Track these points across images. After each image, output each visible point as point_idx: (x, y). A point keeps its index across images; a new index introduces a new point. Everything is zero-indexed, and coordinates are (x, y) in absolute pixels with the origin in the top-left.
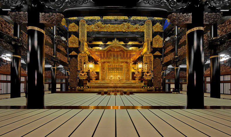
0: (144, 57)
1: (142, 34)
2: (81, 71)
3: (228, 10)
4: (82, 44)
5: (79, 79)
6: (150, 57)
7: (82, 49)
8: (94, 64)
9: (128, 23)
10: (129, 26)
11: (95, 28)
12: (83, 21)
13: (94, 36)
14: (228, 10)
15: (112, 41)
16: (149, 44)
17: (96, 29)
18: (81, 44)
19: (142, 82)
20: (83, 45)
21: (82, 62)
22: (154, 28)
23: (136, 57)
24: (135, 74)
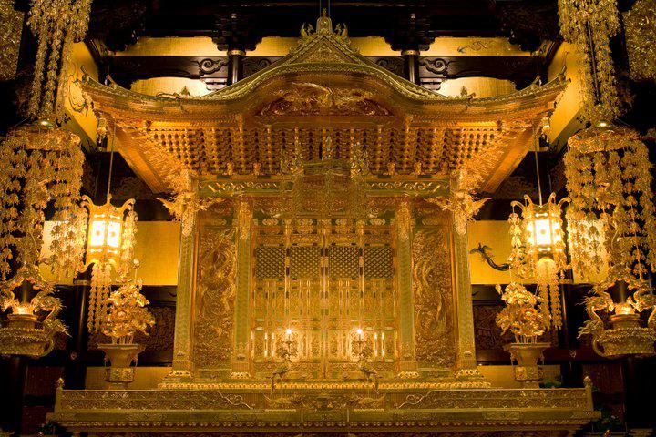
4: (49, 51)
7: (43, 92)
15: (298, 35)
16: (603, 53)
18: (41, 54)
20: (53, 64)
21: (32, 200)
24: (503, 304)
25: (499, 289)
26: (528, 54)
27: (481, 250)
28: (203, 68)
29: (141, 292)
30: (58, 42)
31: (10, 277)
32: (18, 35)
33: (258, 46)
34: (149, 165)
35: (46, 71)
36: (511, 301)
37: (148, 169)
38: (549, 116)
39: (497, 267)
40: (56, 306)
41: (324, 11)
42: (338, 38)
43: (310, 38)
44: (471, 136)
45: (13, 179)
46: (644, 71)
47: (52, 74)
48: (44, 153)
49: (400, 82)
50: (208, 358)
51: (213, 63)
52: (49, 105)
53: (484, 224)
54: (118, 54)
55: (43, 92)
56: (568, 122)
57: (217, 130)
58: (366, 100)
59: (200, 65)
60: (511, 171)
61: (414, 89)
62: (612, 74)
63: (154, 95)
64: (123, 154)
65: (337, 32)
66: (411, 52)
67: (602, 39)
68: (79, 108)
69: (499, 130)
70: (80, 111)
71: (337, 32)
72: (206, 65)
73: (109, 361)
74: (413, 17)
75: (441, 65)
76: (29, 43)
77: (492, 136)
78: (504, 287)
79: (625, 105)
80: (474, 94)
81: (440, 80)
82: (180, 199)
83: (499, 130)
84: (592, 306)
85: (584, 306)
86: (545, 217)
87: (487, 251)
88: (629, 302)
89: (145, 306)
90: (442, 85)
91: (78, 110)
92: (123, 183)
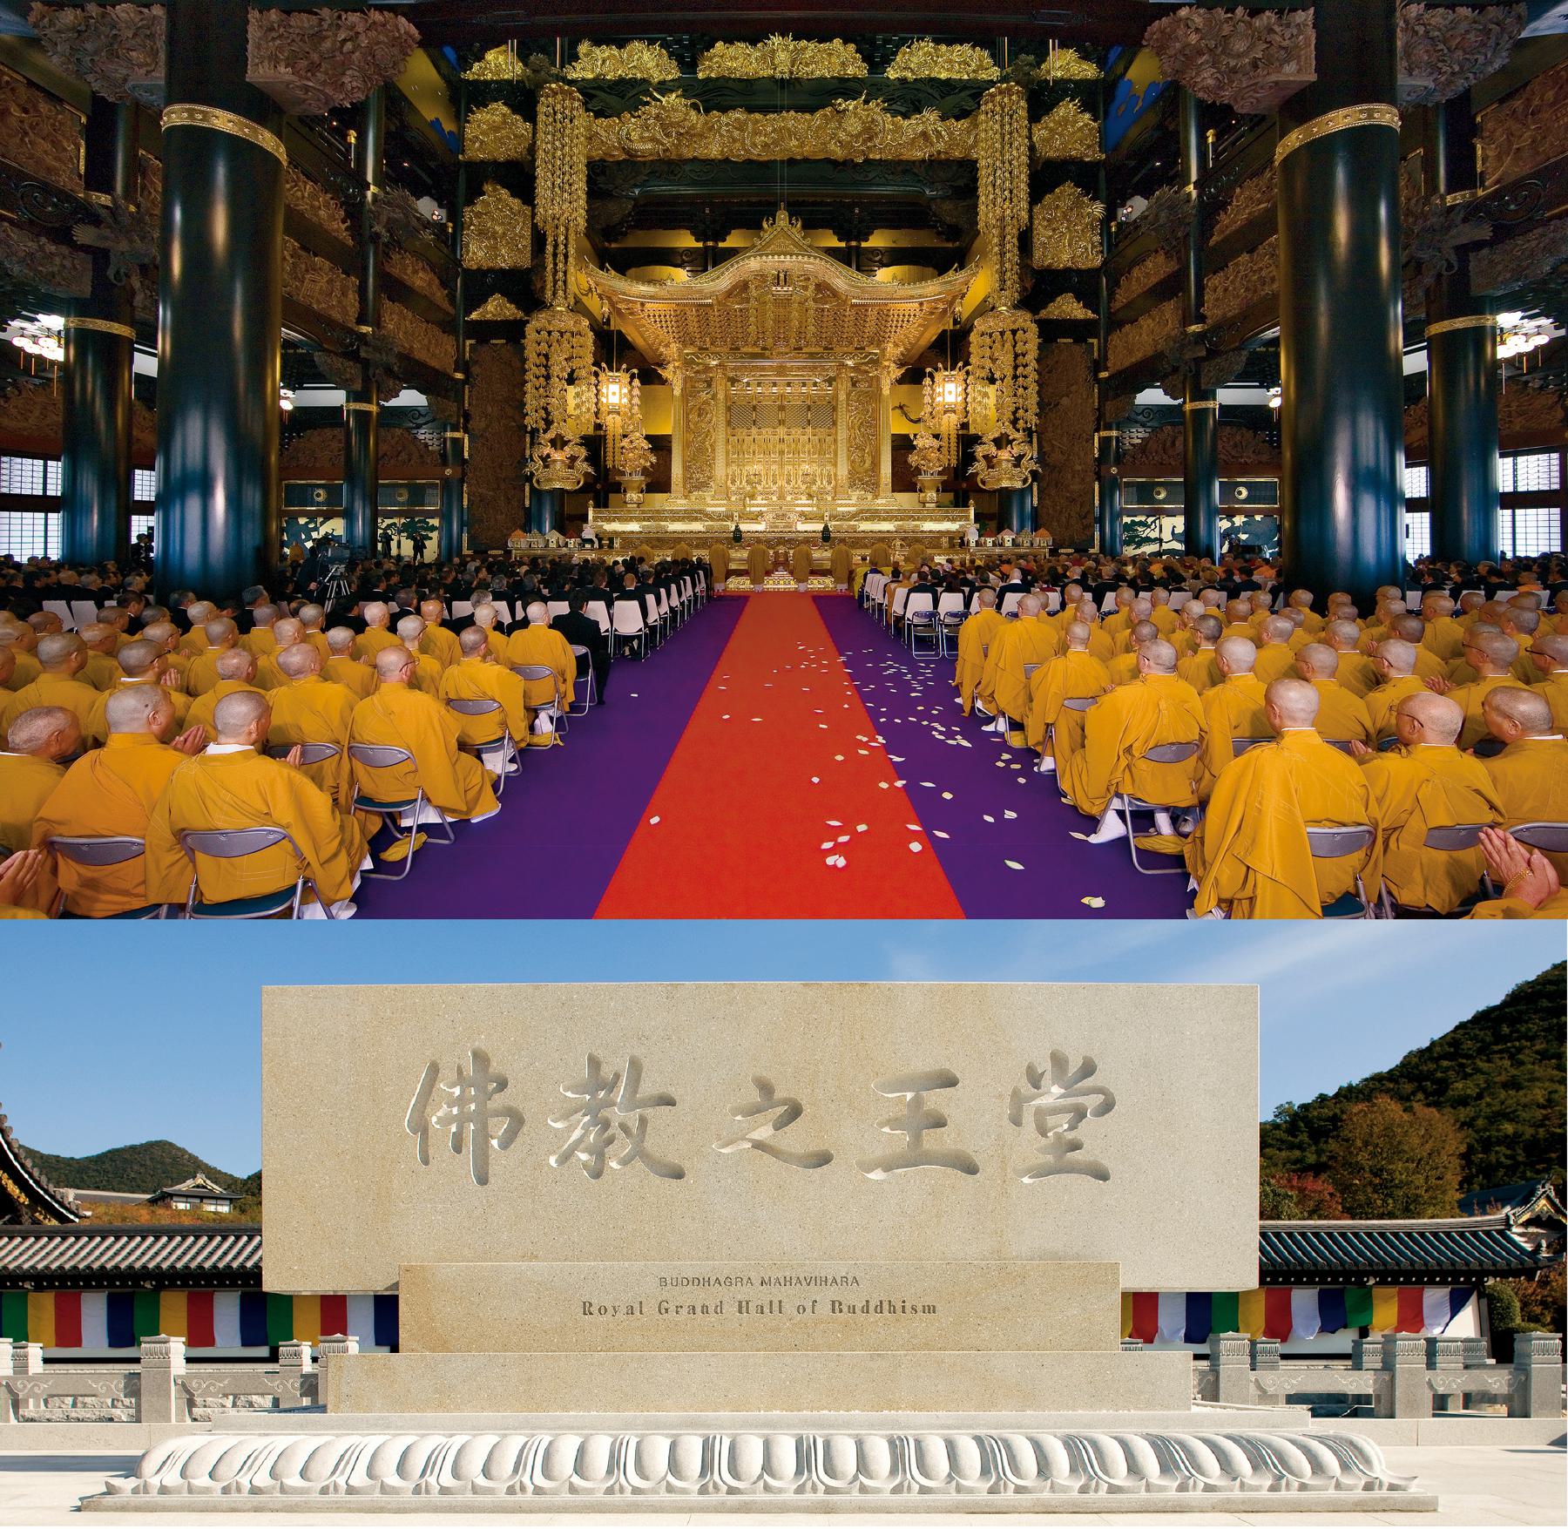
0: (973, 337)
1: (961, 177)
2: (551, 435)
4: (556, 246)
6: (1014, 332)
8: (636, 382)
9: (866, 102)
12: (563, 92)
15: (760, 228)
16: (1012, 242)
17: (649, 146)
18: (549, 248)
21: (555, 370)
22: (1040, 133)
24: (914, 447)
27: (901, 407)
31: (545, 431)
35: (555, 264)
40: (583, 452)
47: (561, 265)
53: (905, 387)
55: (555, 282)
76: (539, 239)
77: (1226, 290)
82: (671, 367)
84: (980, 451)
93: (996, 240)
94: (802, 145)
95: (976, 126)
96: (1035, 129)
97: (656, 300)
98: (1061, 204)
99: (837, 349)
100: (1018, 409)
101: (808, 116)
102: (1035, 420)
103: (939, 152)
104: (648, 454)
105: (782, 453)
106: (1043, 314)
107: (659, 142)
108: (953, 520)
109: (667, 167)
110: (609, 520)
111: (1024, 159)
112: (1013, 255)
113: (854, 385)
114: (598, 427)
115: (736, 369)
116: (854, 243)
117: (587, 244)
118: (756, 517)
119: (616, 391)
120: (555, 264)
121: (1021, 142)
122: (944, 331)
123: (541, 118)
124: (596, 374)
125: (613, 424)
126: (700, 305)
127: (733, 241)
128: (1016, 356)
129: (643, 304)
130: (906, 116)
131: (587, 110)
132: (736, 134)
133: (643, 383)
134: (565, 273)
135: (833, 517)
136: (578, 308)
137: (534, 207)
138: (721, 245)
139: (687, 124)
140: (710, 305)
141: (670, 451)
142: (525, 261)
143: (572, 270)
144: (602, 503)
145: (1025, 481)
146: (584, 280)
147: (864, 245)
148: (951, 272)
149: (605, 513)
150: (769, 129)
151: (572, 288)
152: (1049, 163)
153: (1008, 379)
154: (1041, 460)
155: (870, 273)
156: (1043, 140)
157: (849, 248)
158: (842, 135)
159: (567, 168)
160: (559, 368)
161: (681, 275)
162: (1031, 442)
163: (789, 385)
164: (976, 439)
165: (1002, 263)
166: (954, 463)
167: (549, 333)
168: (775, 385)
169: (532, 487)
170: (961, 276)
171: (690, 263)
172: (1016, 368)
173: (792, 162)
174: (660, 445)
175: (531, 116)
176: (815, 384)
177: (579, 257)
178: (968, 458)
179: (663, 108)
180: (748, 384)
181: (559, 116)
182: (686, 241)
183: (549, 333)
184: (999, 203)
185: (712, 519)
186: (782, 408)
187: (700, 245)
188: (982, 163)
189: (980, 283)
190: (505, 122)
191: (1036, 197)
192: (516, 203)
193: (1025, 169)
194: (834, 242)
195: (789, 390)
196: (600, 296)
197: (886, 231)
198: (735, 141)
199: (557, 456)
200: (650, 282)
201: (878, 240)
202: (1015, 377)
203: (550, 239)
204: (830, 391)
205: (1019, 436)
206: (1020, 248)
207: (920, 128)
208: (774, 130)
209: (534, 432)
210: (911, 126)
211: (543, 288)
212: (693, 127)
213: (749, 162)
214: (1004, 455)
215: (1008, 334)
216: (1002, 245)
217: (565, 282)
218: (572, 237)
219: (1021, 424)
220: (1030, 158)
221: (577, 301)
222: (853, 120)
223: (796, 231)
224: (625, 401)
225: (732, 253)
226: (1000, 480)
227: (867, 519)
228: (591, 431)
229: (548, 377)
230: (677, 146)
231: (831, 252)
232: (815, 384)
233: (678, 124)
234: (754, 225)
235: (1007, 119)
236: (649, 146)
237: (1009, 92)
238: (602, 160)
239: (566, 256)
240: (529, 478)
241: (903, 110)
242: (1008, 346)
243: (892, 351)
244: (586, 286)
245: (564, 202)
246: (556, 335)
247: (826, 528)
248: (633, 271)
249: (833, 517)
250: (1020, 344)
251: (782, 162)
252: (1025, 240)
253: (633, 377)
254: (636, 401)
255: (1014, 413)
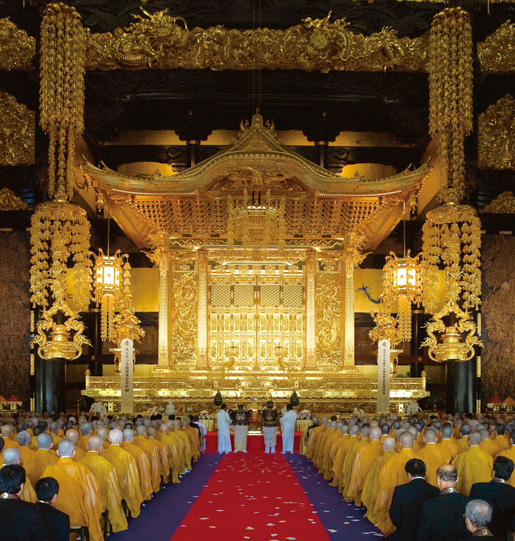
0: (425, 228)
1: (412, 87)
2: (54, 310)
3: (488, 12)
4: (57, 146)
5: (37, 357)
6: (460, 224)
7: (57, 178)
8: (128, 266)
9: (332, 21)
10: (338, 37)
11: (133, 52)
12: (63, 10)
13: (128, 97)
14: (488, 12)
15: (238, 129)
16: (458, 147)
17: (139, 57)
18: (52, 148)
19: (415, 373)
20: (62, 156)
21: (57, 254)
22: (484, 51)
23: (385, 224)
24: (374, 324)
25: (373, 316)
26: (407, 146)
27: (364, 289)
28: (170, 154)
29: (135, 315)
30: (63, 139)
31: (48, 308)
32: (32, 130)
33: (209, 137)
34: (135, 228)
35: (57, 162)
36: (379, 323)
37: (134, 231)
38: (416, 194)
39: (374, 301)
40: (80, 327)
41: (258, 110)
42: (268, 132)
43: (247, 131)
44: (360, 208)
45: (42, 241)
46: (488, 161)
47: (62, 163)
48: (63, 223)
49: (312, 165)
50: (180, 356)
51: (176, 150)
52: (62, 187)
53: (367, 271)
54: (106, 144)
55: (57, 178)
56: (428, 203)
57: (181, 202)
58: (286, 179)
59: (167, 152)
60: (389, 234)
61: (322, 172)
62: (463, 165)
63: (90, 466)
64: (116, 220)
65: (267, 126)
66: (322, 143)
67: (458, 137)
68: (81, 186)
69: (381, 203)
70: (83, 188)
71: (267, 126)
72: (171, 152)
73: (117, 359)
74: (324, 115)
75: (343, 154)
76: (42, 139)
77: (375, 208)
78: (376, 314)
79: (471, 187)
80: (364, 176)
81: (342, 165)
82: (158, 251)
83: (381, 203)
84: (431, 328)
85: (426, 328)
86: (403, 267)
87: (368, 290)
88: (456, 324)
89: (138, 324)
90: (343, 169)
91: (81, 188)
92: (117, 241)
93: (444, 144)
94: (275, 57)
95: (427, 44)
96: (479, 47)
97: (137, 195)
98: (502, 113)
99: (306, 236)
100: (463, 291)
101: (280, 33)
102: (478, 301)
103: (395, 66)
104: (137, 328)
105: (257, 328)
106: (487, 209)
107: (149, 55)
108: (408, 388)
109: (154, 76)
110: (104, 387)
111: (469, 75)
112: (459, 159)
113: (321, 268)
114: (92, 305)
115: (215, 253)
116: (322, 143)
117: (82, 141)
118: (234, 385)
119: (110, 273)
120: (57, 162)
121: (466, 59)
122: (401, 222)
123: (44, 33)
124: (92, 258)
125: (108, 304)
126: (185, 197)
127: (214, 139)
128: (462, 245)
129: (133, 197)
130: (367, 34)
131: (85, 26)
132: (216, 48)
133: (133, 266)
134: (65, 169)
135: (303, 385)
136: (77, 200)
137: (38, 112)
138: (203, 143)
139: (173, 39)
140: (194, 197)
141: (156, 326)
142: (29, 159)
143: (71, 166)
144: (97, 372)
145: (469, 354)
146: (80, 174)
147: (331, 144)
148: (406, 171)
149: (99, 380)
150: (245, 44)
151: (72, 184)
152: (492, 76)
153: (456, 265)
154: (485, 337)
155: (339, 169)
156: (486, 57)
157: (317, 147)
158: (310, 50)
159: (67, 69)
160: (60, 253)
161: (168, 170)
162: (475, 321)
163: (263, 268)
164: (429, 318)
165: (450, 165)
166: (409, 337)
167: (52, 222)
168: (250, 267)
169: (37, 357)
170: (415, 174)
171: (175, 159)
172: (462, 255)
173: (266, 72)
174: (149, 321)
175: (34, 31)
176: (287, 267)
177: (79, 151)
178: (419, 334)
179: (152, 24)
180: (227, 267)
181: (60, 32)
182: (172, 140)
183: (52, 222)
184: (448, 109)
185: (193, 386)
186: (257, 288)
187: (184, 143)
188: (433, 77)
189: (432, 180)
190: (11, 36)
191: (479, 106)
192: (22, 108)
193: (470, 83)
194: (302, 141)
195: (263, 272)
196: (96, 190)
197: (351, 133)
198: (215, 54)
199: (59, 329)
200: (139, 176)
201: (344, 141)
202: (461, 264)
203: (52, 140)
204: (300, 274)
205: (465, 315)
206: (465, 151)
207: (379, 45)
208: (250, 44)
209: (38, 310)
210: (371, 43)
211: (46, 183)
212: (178, 41)
213: (227, 71)
214: (452, 331)
215: (455, 226)
216: (449, 147)
217: (65, 177)
218: (71, 138)
219: (466, 305)
220: (474, 73)
221: (76, 194)
222: (320, 36)
223: (270, 133)
224: (117, 282)
225: (213, 151)
226: (447, 353)
227: (332, 387)
228: (86, 309)
229: (50, 261)
230: (163, 58)
231: (301, 151)
232: (287, 267)
233: (166, 39)
234: (231, 125)
235: (454, 39)
236: (139, 57)
237: (455, 14)
238: (98, 70)
239: (66, 155)
240: (34, 351)
241: (364, 28)
242: (455, 236)
243: (356, 239)
244: (83, 181)
245: (64, 108)
246: (57, 223)
247: (295, 395)
248: (124, 166)
249: (303, 385)
250: (465, 235)
251: (257, 71)
252: (471, 144)
253: (125, 260)
254: (127, 282)
255: (461, 295)
